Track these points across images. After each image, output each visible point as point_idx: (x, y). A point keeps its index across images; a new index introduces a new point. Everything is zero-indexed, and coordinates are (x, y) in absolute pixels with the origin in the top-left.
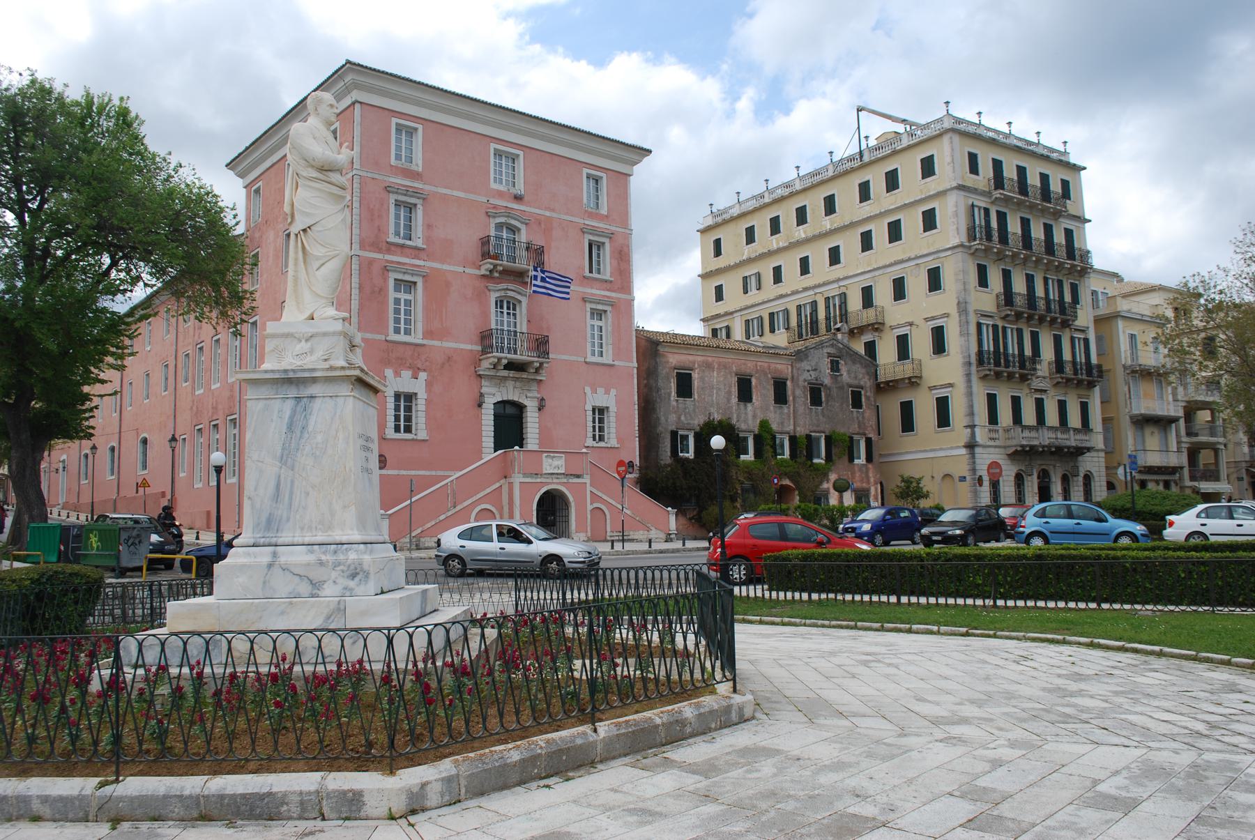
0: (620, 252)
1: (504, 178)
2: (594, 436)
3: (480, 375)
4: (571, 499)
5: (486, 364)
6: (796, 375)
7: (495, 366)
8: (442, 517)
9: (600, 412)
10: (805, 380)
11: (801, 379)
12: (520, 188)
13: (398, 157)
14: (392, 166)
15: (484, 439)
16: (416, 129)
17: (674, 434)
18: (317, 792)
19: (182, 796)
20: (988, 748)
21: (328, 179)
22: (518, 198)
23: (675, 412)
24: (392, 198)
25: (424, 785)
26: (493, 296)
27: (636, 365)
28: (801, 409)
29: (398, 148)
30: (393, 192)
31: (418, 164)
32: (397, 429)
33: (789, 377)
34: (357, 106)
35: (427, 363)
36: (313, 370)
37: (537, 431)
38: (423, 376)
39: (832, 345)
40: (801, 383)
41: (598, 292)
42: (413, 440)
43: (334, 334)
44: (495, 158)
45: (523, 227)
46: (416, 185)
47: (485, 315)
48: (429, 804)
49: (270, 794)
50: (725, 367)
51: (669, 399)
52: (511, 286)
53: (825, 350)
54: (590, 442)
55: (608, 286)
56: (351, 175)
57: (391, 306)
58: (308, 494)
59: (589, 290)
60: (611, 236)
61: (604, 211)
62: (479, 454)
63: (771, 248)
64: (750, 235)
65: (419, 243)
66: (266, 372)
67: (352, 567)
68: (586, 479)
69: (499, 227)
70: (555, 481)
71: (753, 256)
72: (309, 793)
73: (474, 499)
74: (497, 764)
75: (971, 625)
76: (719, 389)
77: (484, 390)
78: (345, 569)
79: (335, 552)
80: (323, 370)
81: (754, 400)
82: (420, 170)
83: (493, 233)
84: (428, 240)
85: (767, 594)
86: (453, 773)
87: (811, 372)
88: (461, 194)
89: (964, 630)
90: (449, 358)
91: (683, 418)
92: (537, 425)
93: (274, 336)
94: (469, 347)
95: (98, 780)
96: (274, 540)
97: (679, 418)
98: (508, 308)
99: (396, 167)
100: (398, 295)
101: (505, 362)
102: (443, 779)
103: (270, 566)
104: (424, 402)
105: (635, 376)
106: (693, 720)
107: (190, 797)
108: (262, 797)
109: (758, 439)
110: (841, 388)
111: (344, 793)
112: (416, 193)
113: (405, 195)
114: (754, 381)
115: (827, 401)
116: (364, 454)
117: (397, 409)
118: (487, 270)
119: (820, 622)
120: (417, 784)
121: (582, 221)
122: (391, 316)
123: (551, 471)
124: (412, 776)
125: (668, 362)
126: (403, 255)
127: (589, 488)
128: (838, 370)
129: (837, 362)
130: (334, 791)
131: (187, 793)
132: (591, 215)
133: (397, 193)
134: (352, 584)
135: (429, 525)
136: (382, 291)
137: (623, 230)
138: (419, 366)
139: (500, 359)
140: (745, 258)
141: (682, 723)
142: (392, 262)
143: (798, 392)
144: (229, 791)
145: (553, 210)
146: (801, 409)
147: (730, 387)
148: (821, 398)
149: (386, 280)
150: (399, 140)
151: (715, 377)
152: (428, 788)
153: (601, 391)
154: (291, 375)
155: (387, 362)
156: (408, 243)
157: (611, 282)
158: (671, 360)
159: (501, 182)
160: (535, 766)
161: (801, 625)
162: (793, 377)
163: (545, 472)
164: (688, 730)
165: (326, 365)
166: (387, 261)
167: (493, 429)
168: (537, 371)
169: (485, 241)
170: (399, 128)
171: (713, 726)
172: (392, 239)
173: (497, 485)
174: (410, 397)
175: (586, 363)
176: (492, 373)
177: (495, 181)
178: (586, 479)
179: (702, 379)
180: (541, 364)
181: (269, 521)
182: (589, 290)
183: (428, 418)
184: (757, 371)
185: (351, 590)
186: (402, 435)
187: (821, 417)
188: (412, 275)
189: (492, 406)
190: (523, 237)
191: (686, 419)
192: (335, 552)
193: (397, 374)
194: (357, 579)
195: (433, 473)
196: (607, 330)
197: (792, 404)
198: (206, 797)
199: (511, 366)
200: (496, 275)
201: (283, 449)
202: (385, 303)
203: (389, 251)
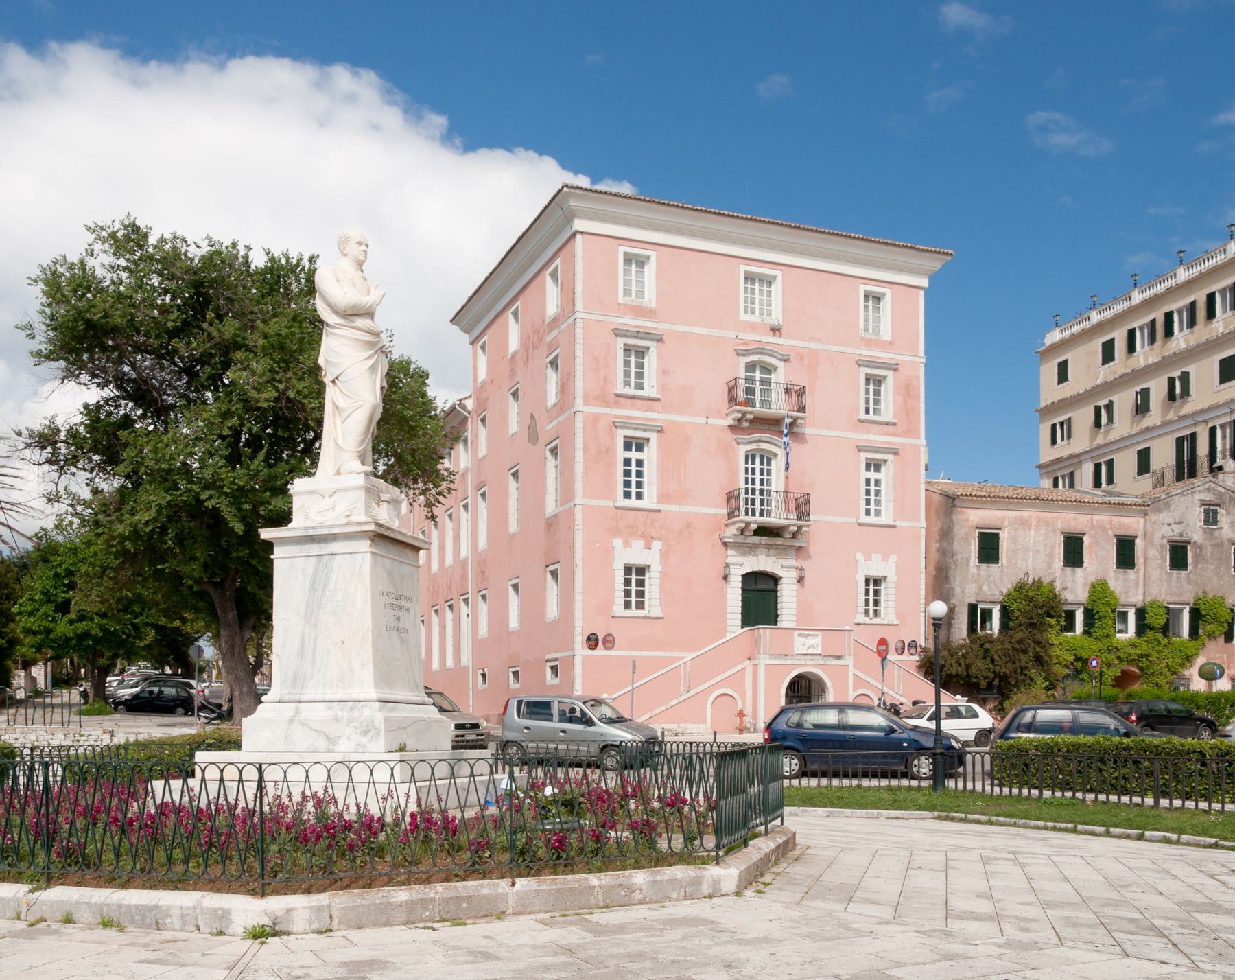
0: (907, 387)
1: (757, 306)
2: (867, 612)
3: (725, 544)
4: (828, 683)
5: (732, 530)
6: (1149, 529)
7: (742, 532)
8: (674, 702)
9: (875, 582)
10: (1163, 537)
11: (1158, 535)
12: (777, 318)
13: (627, 293)
14: (619, 304)
15: (729, 616)
16: (648, 258)
17: (972, 608)
18: (195, 908)
19: (89, 903)
20: (970, 944)
21: (353, 324)
22: (775, 330)
23: (975, 581)
24: (621, 342)
25: (289, 911)
26: (743, 450)
27: (924, 524)
28: (1155, 575)
29: (627, 282)
30: (621, 336)
31: (650, 298)
32: (627, 605)
33: (1140, 533)
34: (579, 237)
35: (663, 531)
36: (331, 526)
37: (795, 606)
38: (657, 545)
39: (1208, 490)
40: (1157, 540)
41: (876, 438)
42: (645, 618)
43: (356, 488)
44: (746, 282)
45: (781, 365)
46: (649, 324)
47: (733, 472)
48: (295, 929)
49: (157, 906)
50: (1047, 524)
51: (968, 565)
52: (764, 436)
53: (1198, 497)
54: (861, 618)
55: (890, 429)
56: (572, 318)
57: (620, 468)
58: (329, 652)
59: (864, 436)
60: (895, 368)
61: (886, 335)
62: (723, 631)
63: (1136, 367)
64: (1108, 353)
65: (650, 391)
66: (294, 529)
67: (365, 724)
68: (849, 661)
69: (750, 367)
70: (809, 662)
71: (1111, 378)
72: (188, 908)
73: (712, 682)
74: (378, 901)
75: (1109, 822)
76: (1037, 552)
77: (730, 560)
78: (358, 725)
79: (352, 709)
80: (340, 526)
81: (1085, 565)
82: (654, 305)
83: (742, 374)
84: (663, 387)
85: (997, 789)
86: (324, 903)
87: (1173, 527)
88: (704, 331)
89: (1213, 840)
90: (688, 525)
91: (985, 588)
92: (794, 599)
93: (300, 493)
94: (712, 511)
95: (30, 886)
96: (297, 697)
97: (980, 589)
98: (762, 463)
99: (625, 305)
100: (628, 454)
101: (754, 526)
102: (311, 908)
103: (291, 721)
104: (658, 575)
105: (923, 538)
106: (644, 887)
107: (96, 904)
108: (151, 909)
109: (1090, 615)
110: (1220, 545)
111: (216, 910)
112: (649, 336)
113: (636, 338)
114: (1086, 540)
115: (1196, 563)
116: (393, 612)
117: (627, 582)
118: (734, 419)
119: (1033, 823)
120: (282, 909)
121: (857, 352)
122: (620, 478)
123: (804, 652)
124: (277, 904)
125: (967, 520)
126: (633, 407)
127: (852, 671)
128: (1215, 522)
129: (1215, 512)
130: (208, 908)
131: (93, 901)
132: (869, 343)
133: (626, 336)
134: (364, 740)
135: (658, 711)
136: (610, 450)
137: (911, 359)
138: (653, 534)
139: (748, 524)
140: (1099, 382)
141: (631, 889)
142: (621, 417)
143: (1152, 552)
144: (126, 902)
145: (820, 341)
146: (1155, 575)
147: (1053, 548)
148: (1186, 559)
149: (613, 438)
150: (626, 272)
151: (1032, 537)
152: (295, 914)
153: (876, 557)
154: (311, 532)
155: (615, 532)
156: (639, 393)
157: (894, 424)
158: (971, 518)
159: (753, 313)
160: (426, 909)
161: (1010, 825)
162: (1145, 534)
163: (796, 652)
164: (637, 896)
165: (346, 520)
166: (616, 416)
167: (740, 604)
168: (794, 535)
169: (732, 386)
170: (628, 259)
171: (674, 895)
172: (621, 390)
173: (740, 667)
174: (641, 571)
175: (860, 525)
176: (741, 539)
177: (746, 312)
178: (849, 661)
179: (1014, 540)
180: (800, 528)
181: (295, 678)
182: (864, 436)
183: (662, 592)
184: (1093, 527)
185: (364, 746)
186: (633, 612)
187: (1185, 585)
188: (645, 430)
189: (740, 579)
190: (779, 378)
191: (990, 588)
192: (352, 709)
193: (627, 544)
194: (369, 736)
195: (669, 654)
196: (887, 483)
197: (1142, 572)
198: (108, 905)
199: (762, 531)
200: (746, 424)
201: (307, 607)
202: (612, 464)
203: (617, 405)
